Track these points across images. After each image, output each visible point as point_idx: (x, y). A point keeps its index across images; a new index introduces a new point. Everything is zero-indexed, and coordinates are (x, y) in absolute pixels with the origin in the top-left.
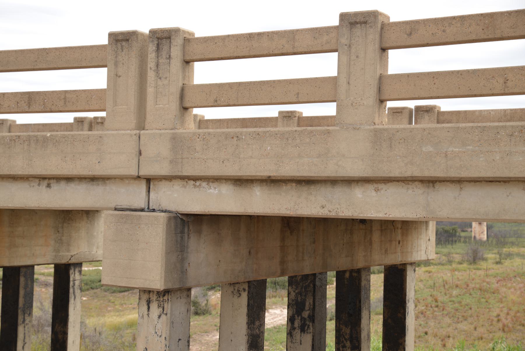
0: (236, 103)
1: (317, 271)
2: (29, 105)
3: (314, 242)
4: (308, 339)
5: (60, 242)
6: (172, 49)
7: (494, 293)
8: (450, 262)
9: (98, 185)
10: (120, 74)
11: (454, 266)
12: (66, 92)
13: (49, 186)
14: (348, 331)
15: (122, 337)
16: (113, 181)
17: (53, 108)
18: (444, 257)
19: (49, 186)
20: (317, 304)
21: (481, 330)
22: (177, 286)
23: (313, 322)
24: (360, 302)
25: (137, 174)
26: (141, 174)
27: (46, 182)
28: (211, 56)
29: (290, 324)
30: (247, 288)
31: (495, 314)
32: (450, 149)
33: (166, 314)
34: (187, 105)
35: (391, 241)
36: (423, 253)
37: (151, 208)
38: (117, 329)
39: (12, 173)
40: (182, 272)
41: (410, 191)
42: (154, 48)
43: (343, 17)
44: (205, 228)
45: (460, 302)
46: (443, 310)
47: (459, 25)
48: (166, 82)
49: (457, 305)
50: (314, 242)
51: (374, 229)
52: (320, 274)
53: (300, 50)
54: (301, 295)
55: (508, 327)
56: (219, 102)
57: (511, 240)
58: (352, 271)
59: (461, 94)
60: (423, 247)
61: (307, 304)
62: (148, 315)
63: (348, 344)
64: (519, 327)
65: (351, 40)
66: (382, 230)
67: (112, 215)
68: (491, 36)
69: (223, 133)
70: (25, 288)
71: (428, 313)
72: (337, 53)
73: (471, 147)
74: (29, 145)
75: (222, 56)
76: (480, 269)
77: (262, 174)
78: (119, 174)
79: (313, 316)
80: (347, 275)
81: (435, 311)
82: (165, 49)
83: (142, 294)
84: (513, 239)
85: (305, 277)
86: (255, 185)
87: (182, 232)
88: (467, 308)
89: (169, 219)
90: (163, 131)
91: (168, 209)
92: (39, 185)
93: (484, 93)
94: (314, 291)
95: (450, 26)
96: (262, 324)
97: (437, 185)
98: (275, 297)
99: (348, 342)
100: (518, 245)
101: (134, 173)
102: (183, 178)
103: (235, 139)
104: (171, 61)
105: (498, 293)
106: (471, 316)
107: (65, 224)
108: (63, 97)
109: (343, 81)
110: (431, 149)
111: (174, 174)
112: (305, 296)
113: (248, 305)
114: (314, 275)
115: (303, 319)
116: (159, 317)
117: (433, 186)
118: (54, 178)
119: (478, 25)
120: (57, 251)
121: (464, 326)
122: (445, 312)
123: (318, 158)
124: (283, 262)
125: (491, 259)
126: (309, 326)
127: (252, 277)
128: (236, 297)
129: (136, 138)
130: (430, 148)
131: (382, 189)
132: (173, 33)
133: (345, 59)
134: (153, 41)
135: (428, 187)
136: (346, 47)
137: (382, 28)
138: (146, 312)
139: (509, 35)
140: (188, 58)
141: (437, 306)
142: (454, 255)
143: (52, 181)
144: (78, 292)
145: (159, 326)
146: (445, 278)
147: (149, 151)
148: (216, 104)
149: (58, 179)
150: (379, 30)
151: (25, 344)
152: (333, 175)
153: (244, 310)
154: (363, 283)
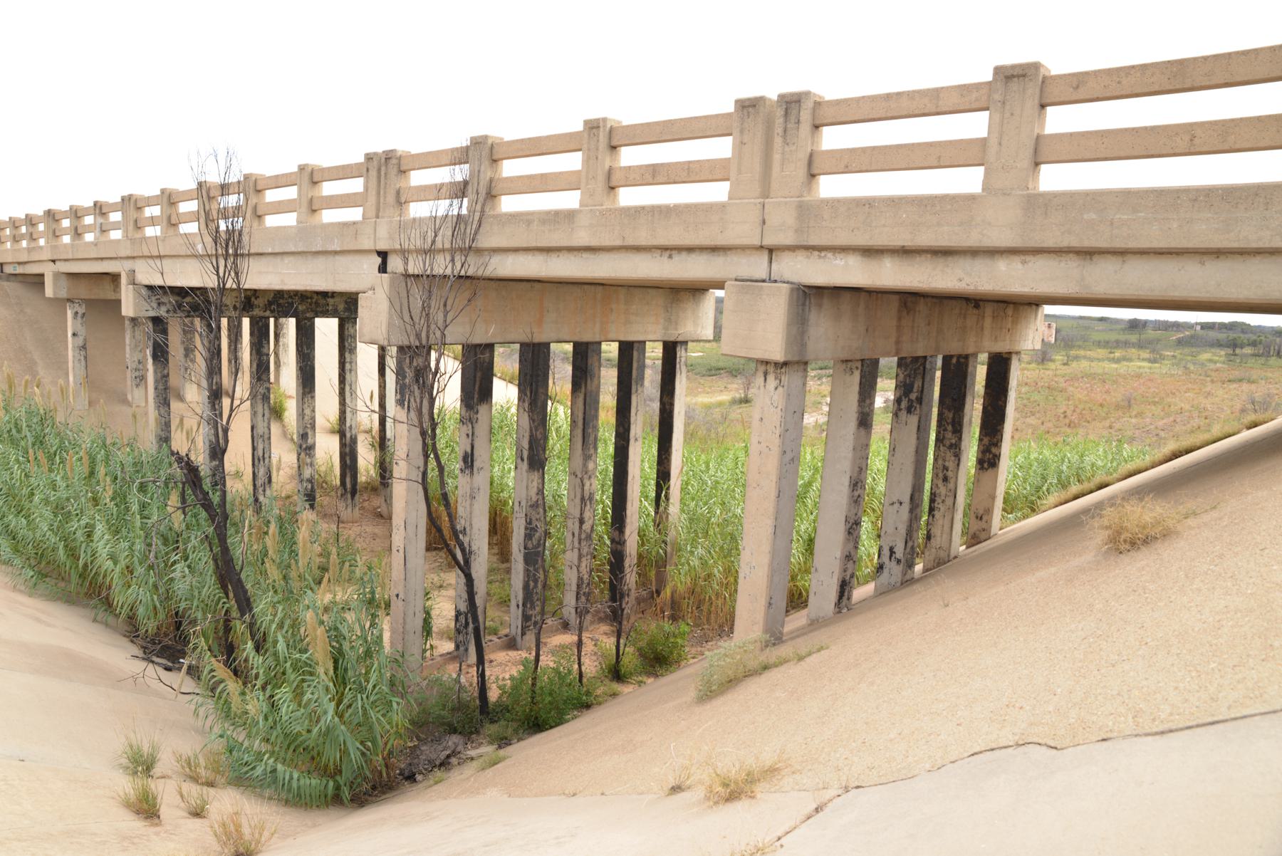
0: (869, 169)
1: (928, 354)
2: (654, 176)
4: (913, 420)
5: (669, 320)
6: (801, 113)
7: (1061, 391)
9: (719, 255)
10: (745, 141)
12: (690, 162)
13: (670, 257)
14: (951, 415)
15: (712, 414)
16: (734, 251)
17: (677, 179)
19: (670, 257)
21: (1050, 425)
22: (796, 359)
23: (921, 404)
24: (966, 387)
26: (764, 243)
27: (668, 253)
29: (896, 405)
30: (860, 366)
31: (1062, 411)
32: (1118, 216)
34: (815, 171)
35: (1001, 328)
36: (1030, 342)
37: (772, 279)
38: (708, 407)
39: (636, 244)
40: (802, 345)
41: (1063, 264)
43: (998, 70)
44: (826, 302)
45: (1029, 399)
47: (1138, 75)
48: (794, 148)
49: (1025, 401)
50: (929, 324)
51: (986, 315)
52: (931, 356)
55: (1074, 422)
56: (850, 168)
57: (1078, 343)
58: (959, 356)
59: (1136, 154)
61: (916, 386)
62: (765, 386)
63: (950, 428)
64: (1084, 424)
65: (1005, 96)
66: (994, 317)
67: (733, 285)
68: (1178, 87)
70: (638, 362)
72: (988, 112)
73: (1143, 214)
74: (653, 216)
75: (856, 118)
76: (1048, 369)
77: (895, 244)
78: (741, 243)
79: (921, 398)
80: (954, 360)
83: (759, 365)
84: (1080, 343)
85: (916, 359)
87: (804, 304)
88: (1035, 404)
89: (792, 290)
90: (788, 199)
91: (790, 280)
92: (661, 256)
93: (1164, 152)
94: (924, 374)
95: (1127, 77)
96: (872, 403)
97: (1096, 258)
99: (950, 426)
100: (1084, 349)
101: (757, 242)
103: (867, 206)
105: (1066, 392)
106: (1038, 412)
107: (674, 305)
108: (686, 167)
109: (993, 148)
111: (799, 244)
113: (860, 383)
115: (910, 401)
116: (776, 388)
117: (1091, 259)
118: (675, 249)
119: (1163, 73)
120: (666, 329)
121: (1032, 420)
123: (960, 226)
124: (898, 342)
125: (1058, 360)
127: (868, 355)
128: (848, 375)
129: (760, 207)
130: (1093, 216)
132: (803, 96)
133: (997, 117)
134: (781, 106)
135: (1085, 259)
136: (999, 104)
137: (1043, 82)
138: (763, 384)
139: (1203, 84)
140: (818, 122)
143: (673, 252)
144: (684, 368)
145: (776, 397)
147: (774, 219)
148: (846, 170)
149: (680, 249)
150: (1040, 83)
151: (637, 411)
152: (977, 245)
153: (856, 388)
154: (970, 369)
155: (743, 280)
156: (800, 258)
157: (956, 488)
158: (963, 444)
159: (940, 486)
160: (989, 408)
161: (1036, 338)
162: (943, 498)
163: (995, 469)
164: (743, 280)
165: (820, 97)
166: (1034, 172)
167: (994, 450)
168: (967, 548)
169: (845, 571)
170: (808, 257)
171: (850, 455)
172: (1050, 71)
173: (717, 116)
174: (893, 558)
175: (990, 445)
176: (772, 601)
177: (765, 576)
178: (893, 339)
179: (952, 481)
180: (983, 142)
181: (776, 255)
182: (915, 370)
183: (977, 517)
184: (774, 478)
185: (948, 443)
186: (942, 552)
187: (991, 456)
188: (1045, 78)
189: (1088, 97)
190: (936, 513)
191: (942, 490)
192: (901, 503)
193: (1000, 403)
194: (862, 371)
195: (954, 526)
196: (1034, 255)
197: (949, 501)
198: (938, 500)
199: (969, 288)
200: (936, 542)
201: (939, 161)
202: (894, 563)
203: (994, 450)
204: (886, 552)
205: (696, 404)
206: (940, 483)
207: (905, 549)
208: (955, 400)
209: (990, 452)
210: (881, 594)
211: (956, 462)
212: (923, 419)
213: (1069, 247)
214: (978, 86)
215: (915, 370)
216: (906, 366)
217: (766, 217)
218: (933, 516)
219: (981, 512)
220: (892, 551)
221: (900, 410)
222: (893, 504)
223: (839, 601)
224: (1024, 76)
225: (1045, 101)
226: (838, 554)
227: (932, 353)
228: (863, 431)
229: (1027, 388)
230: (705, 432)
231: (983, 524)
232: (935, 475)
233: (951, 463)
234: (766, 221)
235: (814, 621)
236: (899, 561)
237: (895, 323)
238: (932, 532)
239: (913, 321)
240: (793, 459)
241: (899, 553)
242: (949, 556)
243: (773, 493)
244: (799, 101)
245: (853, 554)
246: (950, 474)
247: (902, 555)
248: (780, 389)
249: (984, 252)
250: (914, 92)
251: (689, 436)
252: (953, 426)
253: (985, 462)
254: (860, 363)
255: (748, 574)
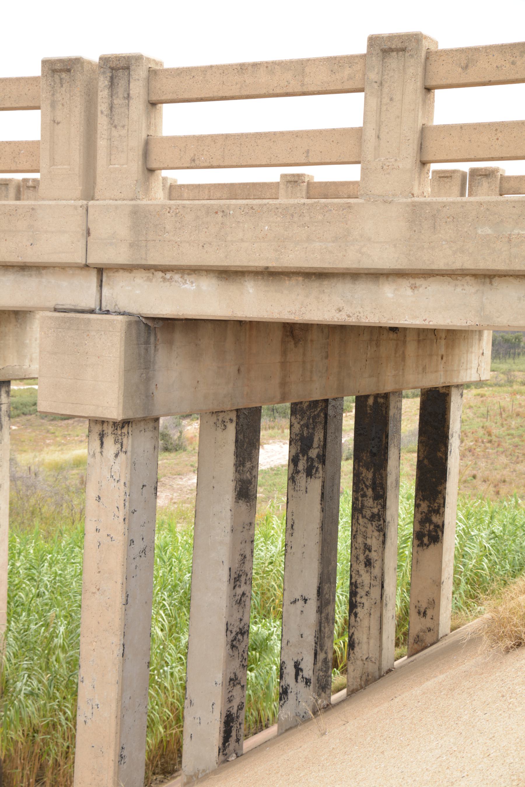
0: (222, 164)
3: (327, 357)
4: (316, 485)
6: (131, 85)
8: (510, 382)
9: (31, 276)
10: (58, 119)
11: (516, 387)
14: (370, 475)
18: (502, 376)
20: (329, 439)
22: (140, 415)
23: (324, 463)
24: (387, 437)
25: (84, 262)
26: (89, 262)
28: (186, 96)
29: (292, 466)
30: (235, 419)
32: (516, 231)
33: (126, 452)
34: (153, 165)
35: (431, 355)
36: (474, 371)
37: (104, 309)
40: (147, 397)
41: (459, 289)
42: (106, 83)
43: (373, 41)
46: (499, 445)
48: (123, 132)
49: (517, 440)
50: (327, 357)
51: (408, 339)
52: (334, 399)
53: (311, 89)
54: (308, 427)
56: (197, 162)
58: (377, 396)
60: (474, 364)
61: (316, 439)
62: (101, 453)
65: (383, 75)
66: (419, 341)
67: (50, 318)
69: (204, 206)
71: (478, 450)
72: (362, 94)
79: (324, 455)
80: (371, 401)
81: (486, 448)
82: (122, 83)
83: (92, 425)
85: (314, 404)
86: (246, 278)
87: (147, 342)
89: (129, 324)
90: (119, 202)
91: (128, 310)
94: (326, 423)
97: (496, 281)
98: (273, 428)
99: (370, 490)
101: (80, 259)
102: (147, 268)
103: (220, 214)
104: (131, 101)
109: (370, 134)
110: (490, 231)
111: (135, 263)
112: (314, 429)
113: (237, 441)
114: (326, 401)
116: (117, 455)
117: (491, 283)
122: (501, 449)
124: (283, 384)
126: (317, 468)
128: (219, 430)
131: (420, 286)
132: (133, 62)
133: (374, 102)
134: (104, 73)
135: (484, 284)
136: (376, 86)
137: (427, 58)
138: (98, 449)
140: (154, 98)
141: (490, 442)
142: (516, 373)
145: (116, 467)
146: (503, 404)
148: (193, 164)
150: (423, 60)
153: (231, 448)
155: (65, 311)
156: (138, 281)
157: (383, 575)
158: (389, 513)
159: (362, 572)
160: (426, 462)
161: (483, 364)
162: (367, 589)
163: (438, 545)
164: (65, 311)
165: (157, 63)
166: (420, 174)
167: (435, 519)
168: (409, 657)
169: (230, 701)
170: (149, 280)
171: (227, 538)
172: (436, 43)
173: (18, 80)
174: (300, 677)
175: (430, 512)
176: (125, 753)
177: (113, 717)
178: (276, 381)
179: (377, 565)
180: (358, 133)
181: (108, 277)
182: (314, 418)
183: (419, 613)
184: (119, 578)
185: (368, 513)
186: (370, 664)
187: (432, 527)
188: (429, 54)
189: (478, 80)
190: (359, 610)
191: (365, 578)
192: (305, 600)
193: (439, 454)
194: (237, 424)
195: (384, 627)
196: (425, 278)
197: (375, 593)
198: (361, 592)
199: (350, 320)
200: (361, 651)
201: (307, 156)
202: (301, 684)
203: (435, 519)
204: (290, 670)
205: (41, 463)
206: (361, 568)
207: (315, 664)
208: (375, 455)
209: (430, 522)
210: (287, 730)
211: (381, 539)
212: (328, 484)
213: (462, 270)
214: (350, 60)
215: (314, 418)
216: (303, 412)
217: (91, 226)
218: (356, 615)
219: (424, 605)
220: (298, 669)
221: (298, 472)
222: (295, 602)
223: (224, 744)
224: (404, 50)
225: (431, 83)
226: (219, 677)
227: (334, 395)
228: (243, 505)
229: (519, 420)
230: (53, 508)
231: (427, 622)
232: (355, 558)
233: (374, 539)
234: (91, 231)
235: (191, 777)
236: (307, 682)
237: (278, 358)
238: (355, 637)
239: (304, 354)
240: (144, 551)
241: (308, 670)
242: (380, 669)
243: (119, 599)
244: (128, 68)
245: (239, 675)
246: (373, 555)
247: (311, 673)
248: (122, 456)
249: (366, 274)
250: (274, 63)
251: (29, 515)
252: (374, 489)
253: (424, 535)
254: (235, 413)
255: (89, 715)
